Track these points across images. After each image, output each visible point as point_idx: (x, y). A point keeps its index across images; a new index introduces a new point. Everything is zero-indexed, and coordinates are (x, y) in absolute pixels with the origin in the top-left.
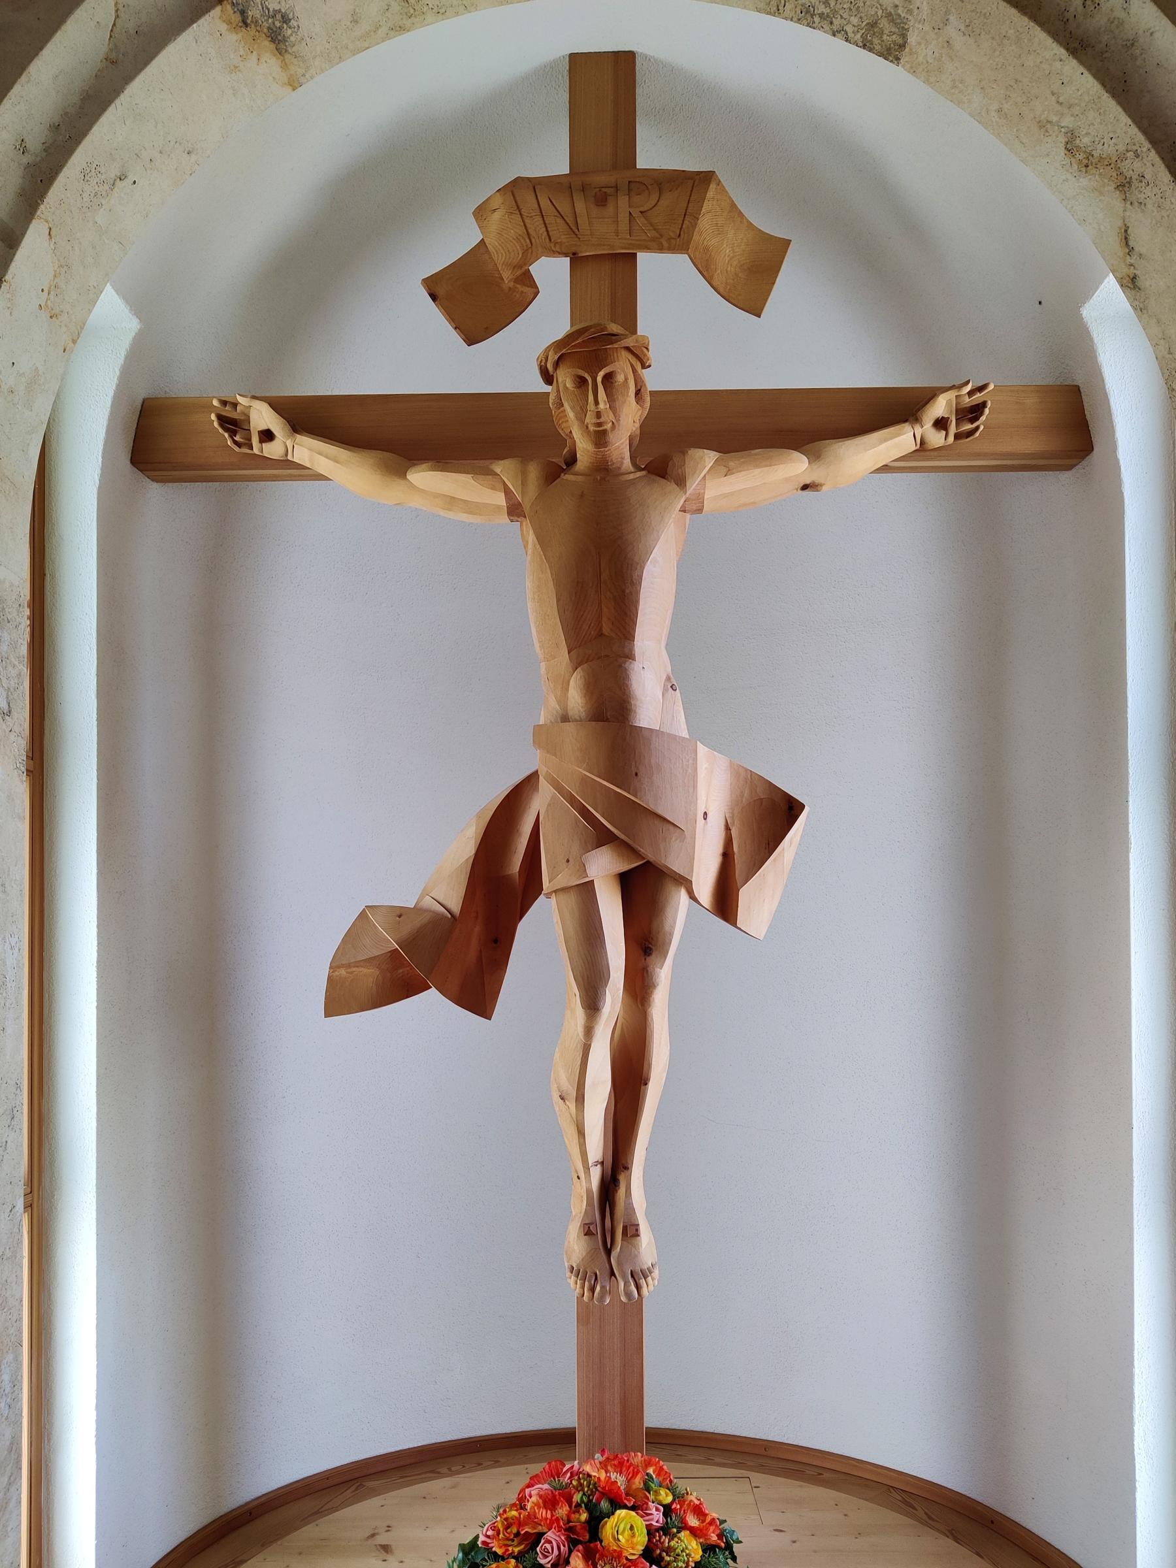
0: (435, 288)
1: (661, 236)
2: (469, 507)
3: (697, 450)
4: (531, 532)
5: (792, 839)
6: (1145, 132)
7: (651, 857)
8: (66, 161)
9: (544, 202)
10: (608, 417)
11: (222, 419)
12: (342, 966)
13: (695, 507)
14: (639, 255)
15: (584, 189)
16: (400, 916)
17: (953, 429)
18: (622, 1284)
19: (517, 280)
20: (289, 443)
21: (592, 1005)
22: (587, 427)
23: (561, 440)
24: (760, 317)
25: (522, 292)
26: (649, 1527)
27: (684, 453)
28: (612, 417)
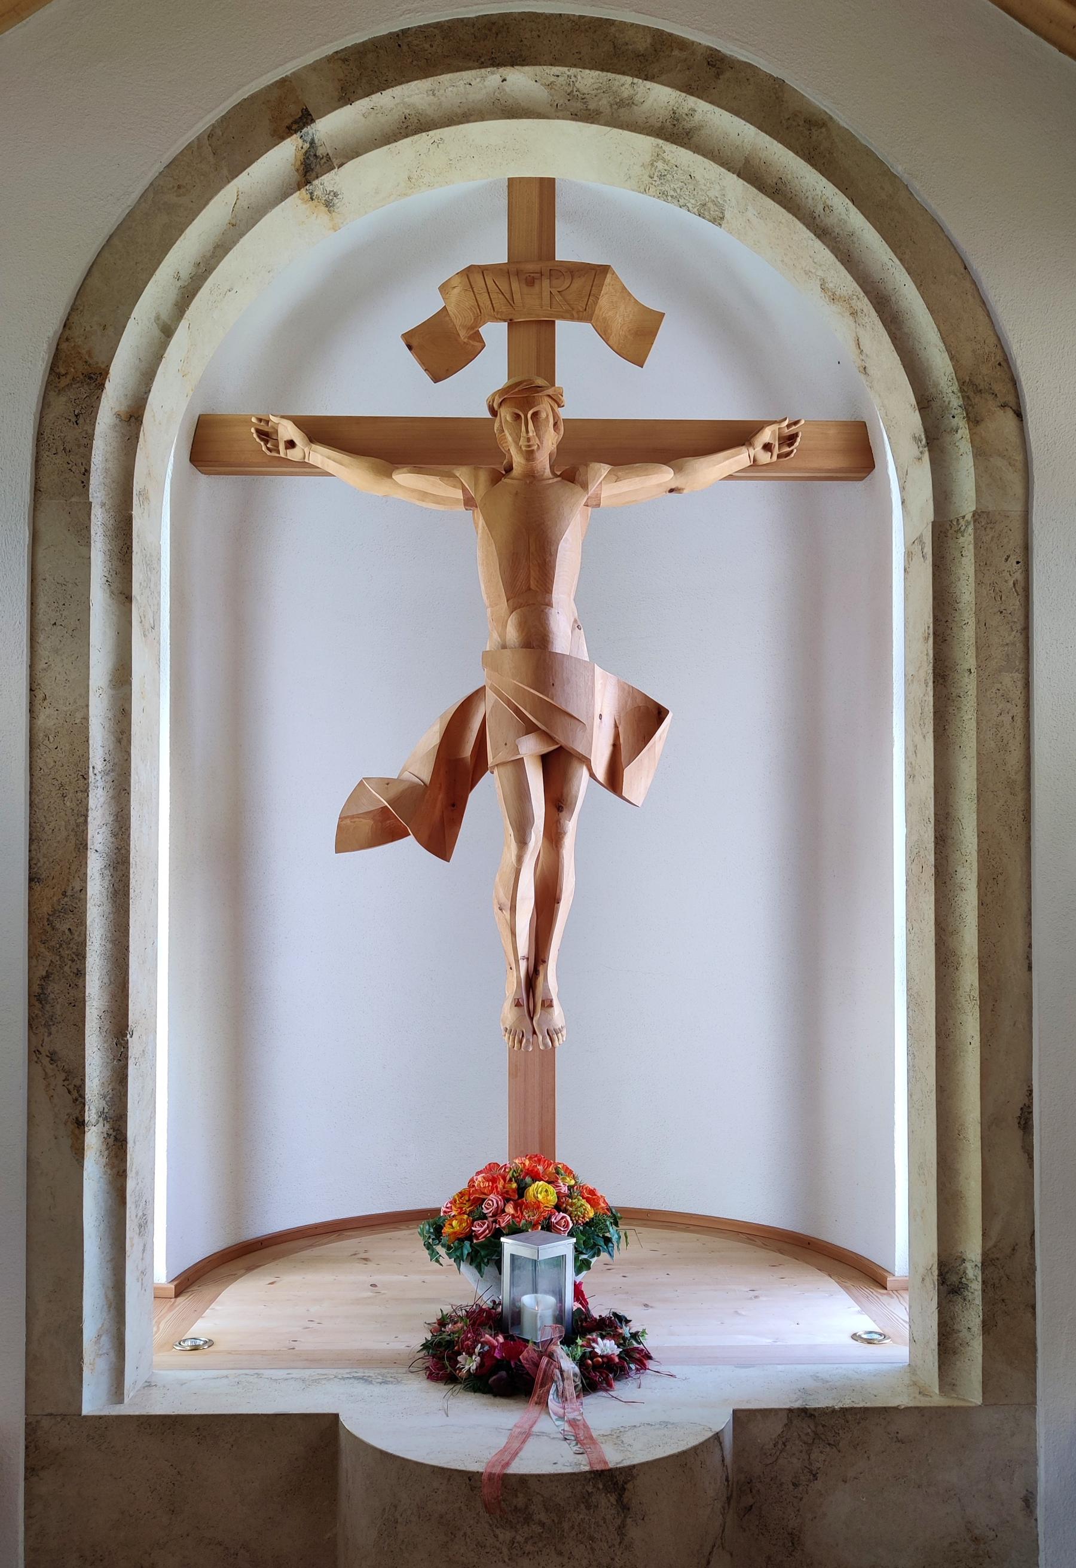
0: (413, 341)
1: (573, 309)
2: (438, 500)
3: (596, 464)
4: (481, 518)
5: (661, 734)
6: (861, 286)
7: (562, 740)
8: (203, 285)
9: (490, 282)
10: (535, 441)
11: (259, 432)
12: (346, 818)
13: (595, 503)
14: (557, 322)
15: (518, 273)
16: (388, 784)
17: (776, 451)
18: (540, 1038)
19: (470, 338)
20: (306, 450)
21: (522, 842)
22: (521, 447)
23: (497, 452)
24: (642, 367)
25: (473, 345)
26: (558, 1194)
27: (587, 465)
28: (538, 441)
